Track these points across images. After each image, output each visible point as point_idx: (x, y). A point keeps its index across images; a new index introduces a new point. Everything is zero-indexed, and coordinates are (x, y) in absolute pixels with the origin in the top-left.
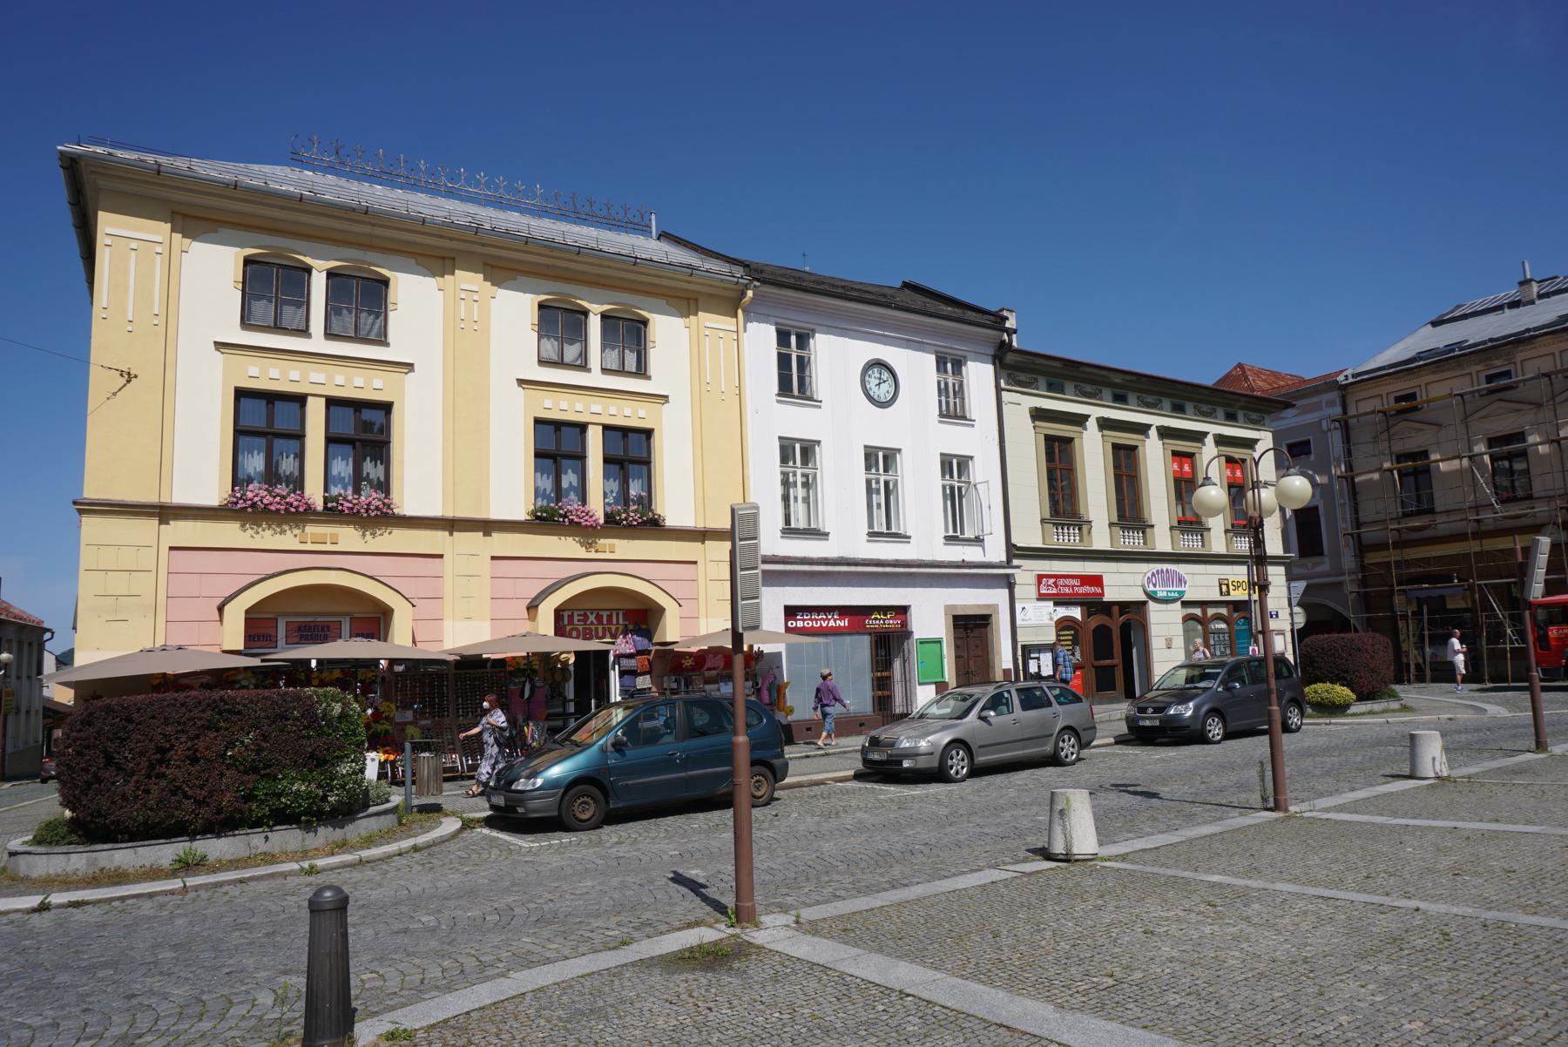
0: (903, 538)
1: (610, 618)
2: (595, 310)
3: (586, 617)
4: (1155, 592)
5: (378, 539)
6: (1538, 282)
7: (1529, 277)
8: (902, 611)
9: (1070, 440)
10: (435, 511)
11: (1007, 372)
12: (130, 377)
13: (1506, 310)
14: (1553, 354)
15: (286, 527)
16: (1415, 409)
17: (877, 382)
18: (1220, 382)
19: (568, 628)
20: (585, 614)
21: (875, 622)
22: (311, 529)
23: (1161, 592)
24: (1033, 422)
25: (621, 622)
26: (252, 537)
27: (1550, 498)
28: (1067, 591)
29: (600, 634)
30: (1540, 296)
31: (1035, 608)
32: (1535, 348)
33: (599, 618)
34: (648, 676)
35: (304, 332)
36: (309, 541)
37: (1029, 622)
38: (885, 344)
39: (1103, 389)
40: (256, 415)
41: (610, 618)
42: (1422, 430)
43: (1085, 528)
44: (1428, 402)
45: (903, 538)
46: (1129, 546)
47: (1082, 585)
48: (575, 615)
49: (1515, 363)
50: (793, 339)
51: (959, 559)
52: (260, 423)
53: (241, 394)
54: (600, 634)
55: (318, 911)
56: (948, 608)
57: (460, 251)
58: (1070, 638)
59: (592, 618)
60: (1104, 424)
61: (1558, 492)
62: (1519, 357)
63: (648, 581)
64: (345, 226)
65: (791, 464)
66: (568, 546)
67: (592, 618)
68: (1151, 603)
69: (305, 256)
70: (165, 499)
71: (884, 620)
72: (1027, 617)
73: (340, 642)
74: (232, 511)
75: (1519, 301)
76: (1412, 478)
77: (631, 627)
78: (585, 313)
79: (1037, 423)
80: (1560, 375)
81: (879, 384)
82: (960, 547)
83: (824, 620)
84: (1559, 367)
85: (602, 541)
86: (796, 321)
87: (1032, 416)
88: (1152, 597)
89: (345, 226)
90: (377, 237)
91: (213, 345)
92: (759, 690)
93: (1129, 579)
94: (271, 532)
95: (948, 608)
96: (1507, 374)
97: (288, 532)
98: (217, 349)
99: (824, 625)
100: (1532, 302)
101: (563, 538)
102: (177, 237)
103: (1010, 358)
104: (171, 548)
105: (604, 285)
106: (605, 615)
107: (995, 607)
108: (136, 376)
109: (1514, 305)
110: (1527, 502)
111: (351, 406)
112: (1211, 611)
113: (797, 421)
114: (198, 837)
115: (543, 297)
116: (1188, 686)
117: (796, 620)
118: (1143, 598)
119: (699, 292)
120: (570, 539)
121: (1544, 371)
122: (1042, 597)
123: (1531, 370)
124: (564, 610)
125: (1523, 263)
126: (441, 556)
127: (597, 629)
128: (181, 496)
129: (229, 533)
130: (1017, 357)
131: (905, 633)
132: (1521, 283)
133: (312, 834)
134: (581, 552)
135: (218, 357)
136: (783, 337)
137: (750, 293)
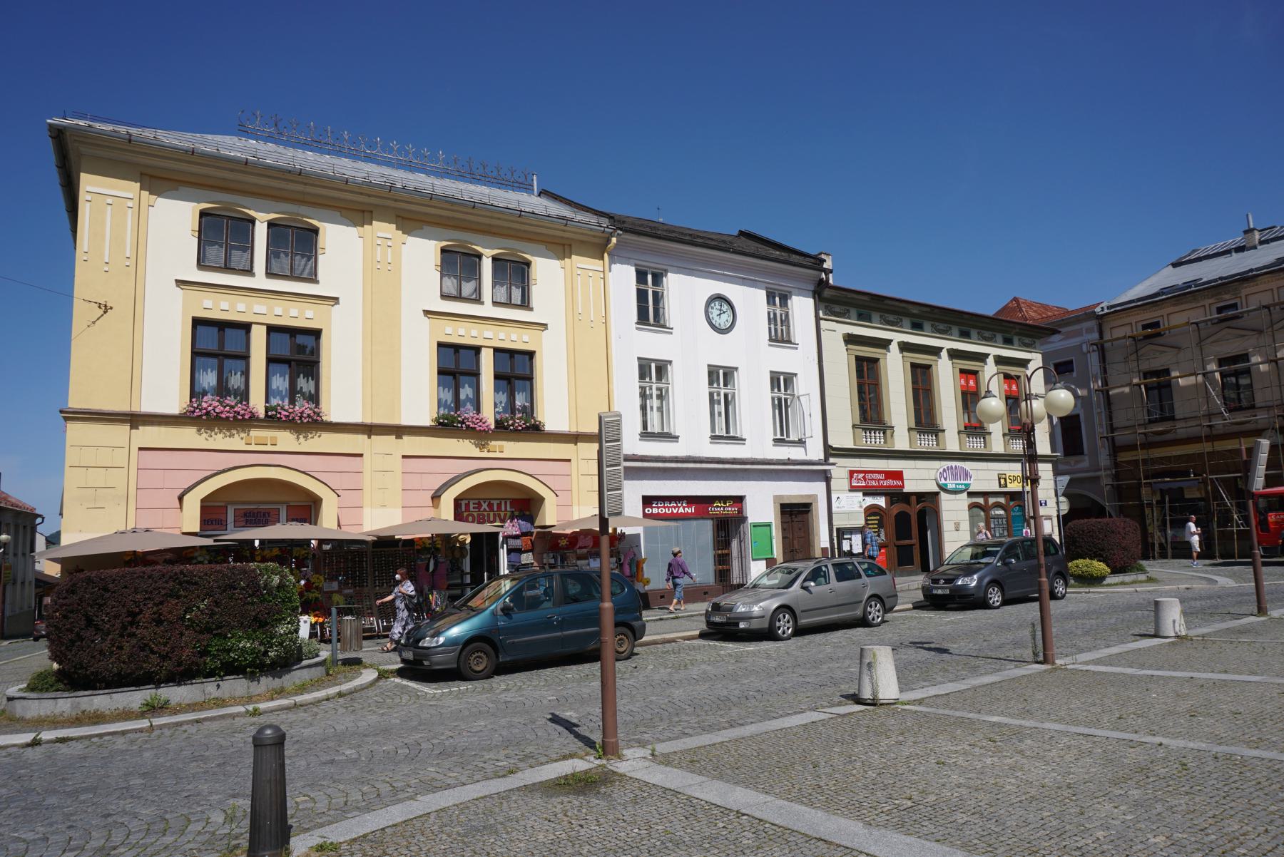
0: (739, 440)
1: (499, 506)
2: (488, 254)
3: (480, 505)
4: (946, 485)
5: (310, 441)
6: (1260, 231)
7: (1252, 226)
8: (739, 500)
9: (876, 360)
10: (356, 418)
11: (824, 304)
12: (106, 309)
13: (1233, 254)
14: (1272, 290)
15: (234, 432)
16: (1159, 335)
17: (718, 312)
18: (999, 312)
19: (465, 514)
20: (479, 503)
21: (716, 509)
22: (255, 433)
23: (951, 485)
24: (846, 346)
25: (508, 509)
26: (206, 439)
27: (1269, 408)
28: (874, 484)
29: (492, 519)
30: (1261, 243)
31: (847, 497)
32: (1257, 285)
33: (490, 506)
34: (531, 554)
35: (249, 272)
36: (253, 443)
37: (843, 509)
38: (725, 281)
39: (903, 318)
40: (210, 340)
41: (499, 506)
42: (1165, 352)
43: (888, 432)
44: (1169, 329)
45: (739, 440)
46: (924, 447)
47: (886, 479)
48: (471, 503)
49: (1240, 297)
50: (650, 277)
51: (785, 457)
52: (213, 346)
53: (197, 322)
54: (492, 519)
55: (260, 746)
56: (776, 497)
57: (377, 206)
58: (877, 522)
59: (485, 506)
60: (904, 347)
61: (1276, 403)
62: (1244, 292)
63: (531, 476)
64: (283, 185)
65: (648, 380)
66: (465, 447)
67: (485, 506)
68: (942, 493)
69: (250, 209)
70: (135, 409)
71: (724, 507)
72: (841, 505)
73: (278, 525)
74: (190, 419)
75: (1244, 246)
76: (1156, 391)
77: (516, 513)
78: (479, 256)
79: (850, 346)
80: (1277, 307)
81: (720, 314)
82: (786, 448)
83: (675, 508)
84: (1277, 301)
85: (493, 443)
86: (652, 262)
87: (845, 341)
88: (943, 488)
89: (283, 185)
90: (309, 194)
91: (174, 283)
92: (621, 565)
93: (925, 474)
94: (222, 435)
95: (776, 497)
96: (1234, 306)
97: (236, 436)
98: (178, 286)
99: (675, 512)
100: (1255, 247)
101: (461, 440)
102: (145, 194)
103: (827, 293)
104: (140, 449)
105: (494, 233)
106: (495, 503)
107: (815, 497)
108: (111, 308)
109: (1240, 249)
110: (1251, 411)
111: (287, 333)
112: (992, 500)
113: (653, 345)
114: (162, 685)
115: (445, 243)
116: (973, 561)
117: (652, 508)
118: (936, 489)
119: (572, 239)
120: (467, 441)
121: (1264, 303)
122: (853, 489)
123: (1254, 303)
124: (462, 500)
125: (1247, 215)
126: (361, 455)
127: (489, 515)
128: (148, 406)
129: (188, 436)
130: (833, 293)
131: (741, 518)
132: (1246, 232)
133: (256, 683)
134: (476, 452)
135: (179, 292)
136: (641, 276)
137: (614, 240)
